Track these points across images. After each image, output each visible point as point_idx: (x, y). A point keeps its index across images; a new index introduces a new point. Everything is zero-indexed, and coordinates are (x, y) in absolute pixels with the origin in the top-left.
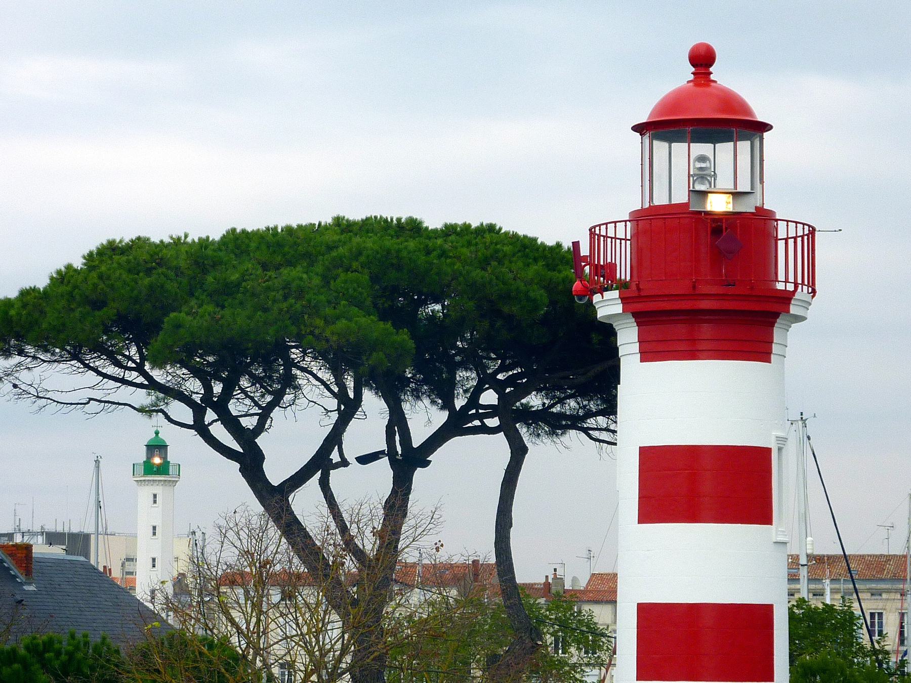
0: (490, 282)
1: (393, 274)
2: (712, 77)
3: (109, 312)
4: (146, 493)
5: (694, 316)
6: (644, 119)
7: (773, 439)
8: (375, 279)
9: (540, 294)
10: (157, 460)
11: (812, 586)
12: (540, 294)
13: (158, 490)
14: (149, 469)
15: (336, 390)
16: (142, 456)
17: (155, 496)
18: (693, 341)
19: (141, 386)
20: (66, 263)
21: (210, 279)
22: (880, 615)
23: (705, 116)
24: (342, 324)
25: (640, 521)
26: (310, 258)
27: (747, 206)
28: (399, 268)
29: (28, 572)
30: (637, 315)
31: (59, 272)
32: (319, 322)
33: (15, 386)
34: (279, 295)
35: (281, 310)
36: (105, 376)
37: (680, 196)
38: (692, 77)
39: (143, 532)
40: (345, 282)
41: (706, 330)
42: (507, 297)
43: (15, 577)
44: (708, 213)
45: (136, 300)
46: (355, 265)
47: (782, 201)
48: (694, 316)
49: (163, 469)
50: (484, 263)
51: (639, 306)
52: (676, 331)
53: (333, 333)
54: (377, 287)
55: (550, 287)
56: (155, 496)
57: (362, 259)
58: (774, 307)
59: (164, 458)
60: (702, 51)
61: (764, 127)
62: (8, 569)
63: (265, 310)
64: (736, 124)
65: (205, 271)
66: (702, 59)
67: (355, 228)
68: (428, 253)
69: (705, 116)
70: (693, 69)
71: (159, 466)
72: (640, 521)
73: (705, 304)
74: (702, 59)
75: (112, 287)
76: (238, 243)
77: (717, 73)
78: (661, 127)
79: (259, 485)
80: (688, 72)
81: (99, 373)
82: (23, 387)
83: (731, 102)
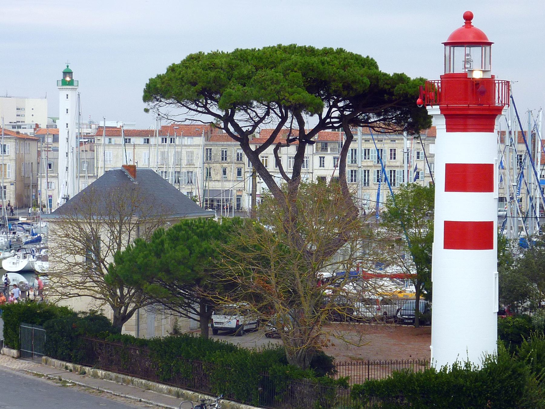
0: (348, 76)
1: (311, 73)
2: (472, 24)
3: (199, 87)
4: (63, 94)
5: (466, 117)
6: (446, 41)
7: (494, 161)
8: (304, 75)
9: (366, 80)
10: (68, 79)
11: (364, 137)
12: (366, 80)
13: (69, 92)
14: (64, 83)
15: (280, 115)
16: (61, 77)
17: (67, 95)
18: (466, 125)
19: (205, 113)
20: (172, 63)
21: (236, 73)
22: (395, 150)
23: (468, 38)
24: (296, 96)
25: (445, 191)
26: (274, 65)
27: (488, 76)
28: (313, 71)
29: (135, 176)
30: (447, 116)
31: (170, 67)
32: (287, 94)
33: (159, 115)
34: (269, 83)
35: (271, 90)
36: (190, 109)
37: (462, 71)
38: (464, 24)
39: (62, 112)
40: (293, 76)
41: (470, 121)
42: (354, 82)
43: (130, 178)
44: (473, 78)
45: (209, 82)
46: (295, 69)
47: (499, 73)
48: (466, 117)
49: (71, 83)
50: (344, 68)
51: (447, 112)
52: (457, 122)
53: (293, 99)
54: (304, 78)
55: (369, 77)
56: (67, 95)
57: (298, 66)
58: (494, 113)
59: (71, 78)
60: (469, 14)
61: (490, 44)
62: (127, 175)
63: (265, 89)
64: (482, 42)
65: (233, 69)
66: (468, 17)
67: (288, 50)
68: (323, 63)
69: (468, 38)
70: (465, 21)
71: (69, 81)
72: (445, 191)
73: (470, 112)
74: (468, 17)
75: (199, 77)
76: (242, 56)
77: (473, 22)
78: (452, 44)
79: (248, 151)
80: (463, 22)
81: (188, 108)
82: (162, 115)
83: (480, 34)
